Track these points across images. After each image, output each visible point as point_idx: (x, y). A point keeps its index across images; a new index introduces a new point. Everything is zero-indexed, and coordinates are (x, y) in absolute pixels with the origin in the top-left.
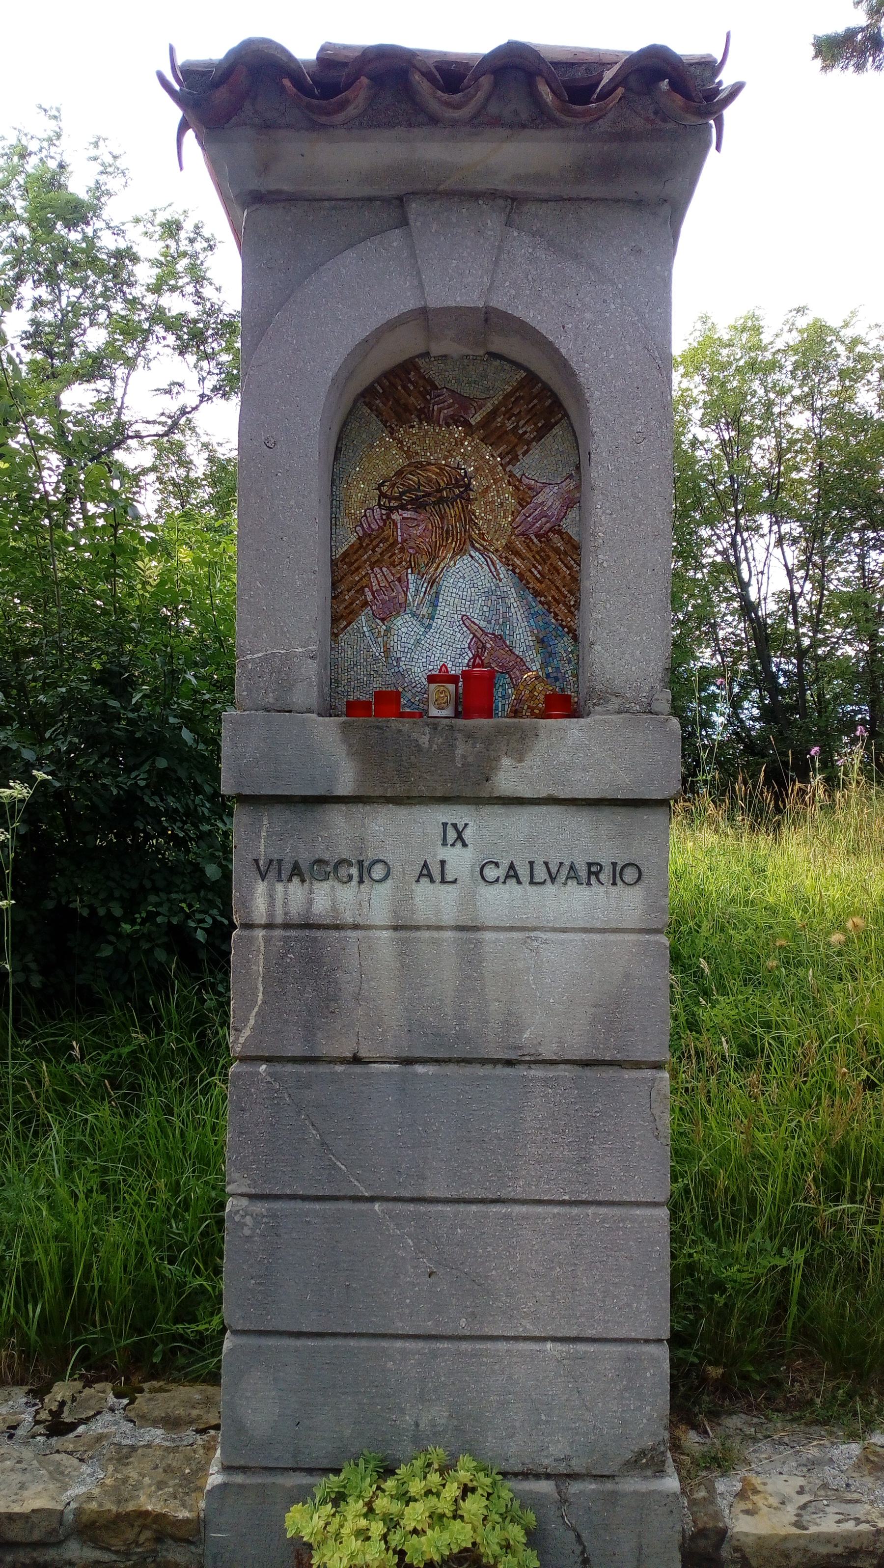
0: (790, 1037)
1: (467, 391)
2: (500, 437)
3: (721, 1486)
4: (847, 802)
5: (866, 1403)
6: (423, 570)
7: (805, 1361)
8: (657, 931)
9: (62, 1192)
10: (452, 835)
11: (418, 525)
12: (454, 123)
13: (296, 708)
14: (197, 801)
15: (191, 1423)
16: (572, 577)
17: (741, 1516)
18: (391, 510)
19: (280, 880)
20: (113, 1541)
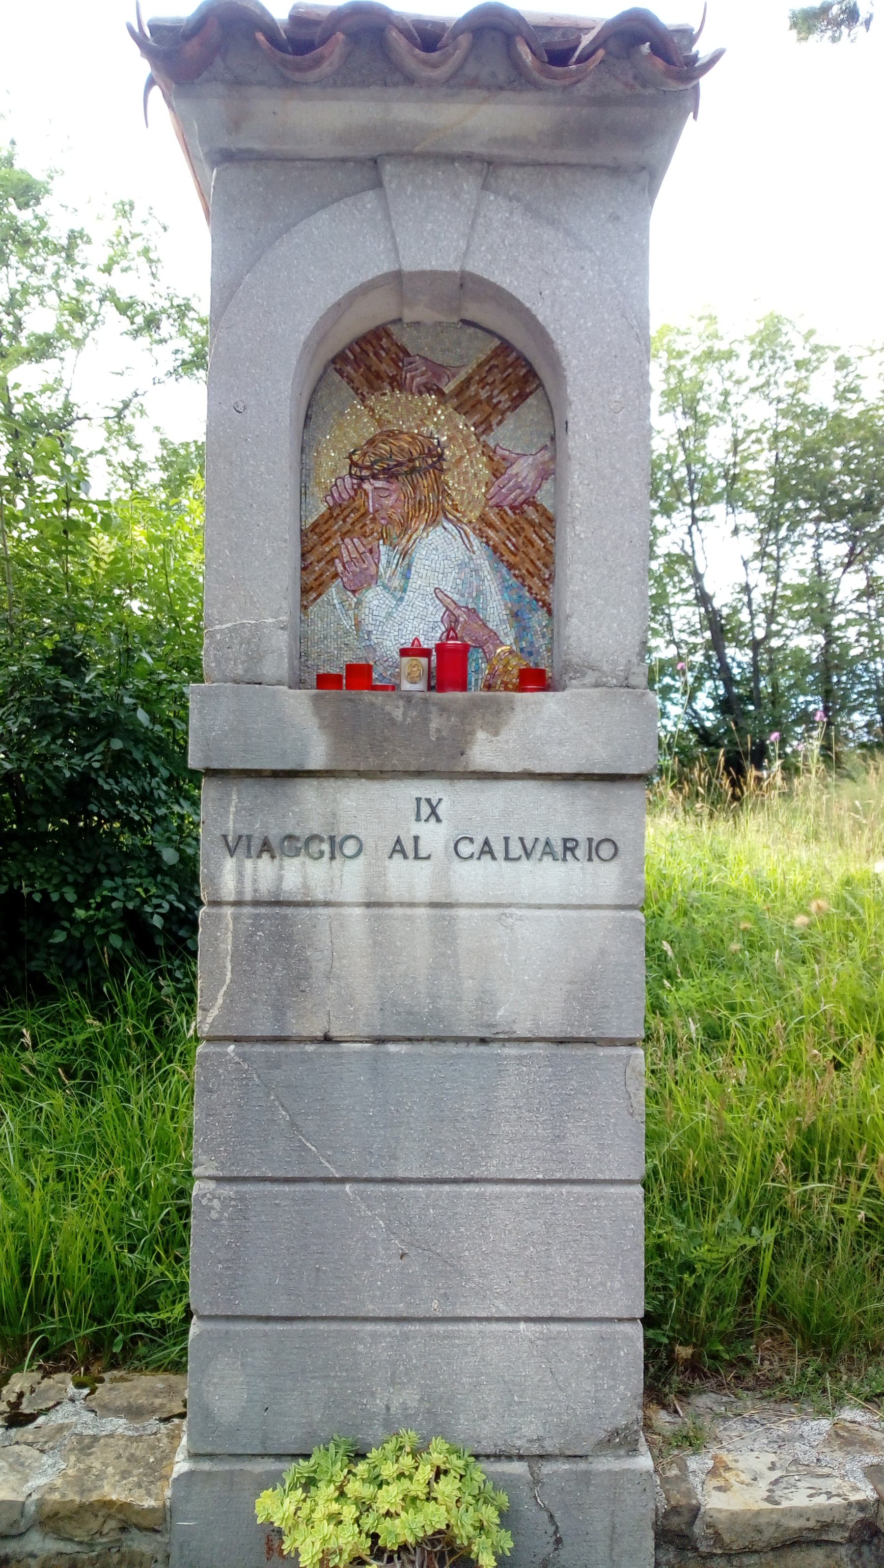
0: (756, 1019)
1: (439, 358)
2: (473, 406)
3: (693, 1464)
4: (806, 788)
5: (837, 1380)
6: (395, 541)
7: (774, 1340)
8: (632, 907)
9: (18, 1181)
10: (425, 810)
11: (389, 495)
12: (430, 84)
13: (267, 680)
14: (154, 784)
15: (154, 1412)
16: (547, 550)
17: (715, 1493)
18: (362, 479)
19: (249, 856)
20: (78, 1532)
